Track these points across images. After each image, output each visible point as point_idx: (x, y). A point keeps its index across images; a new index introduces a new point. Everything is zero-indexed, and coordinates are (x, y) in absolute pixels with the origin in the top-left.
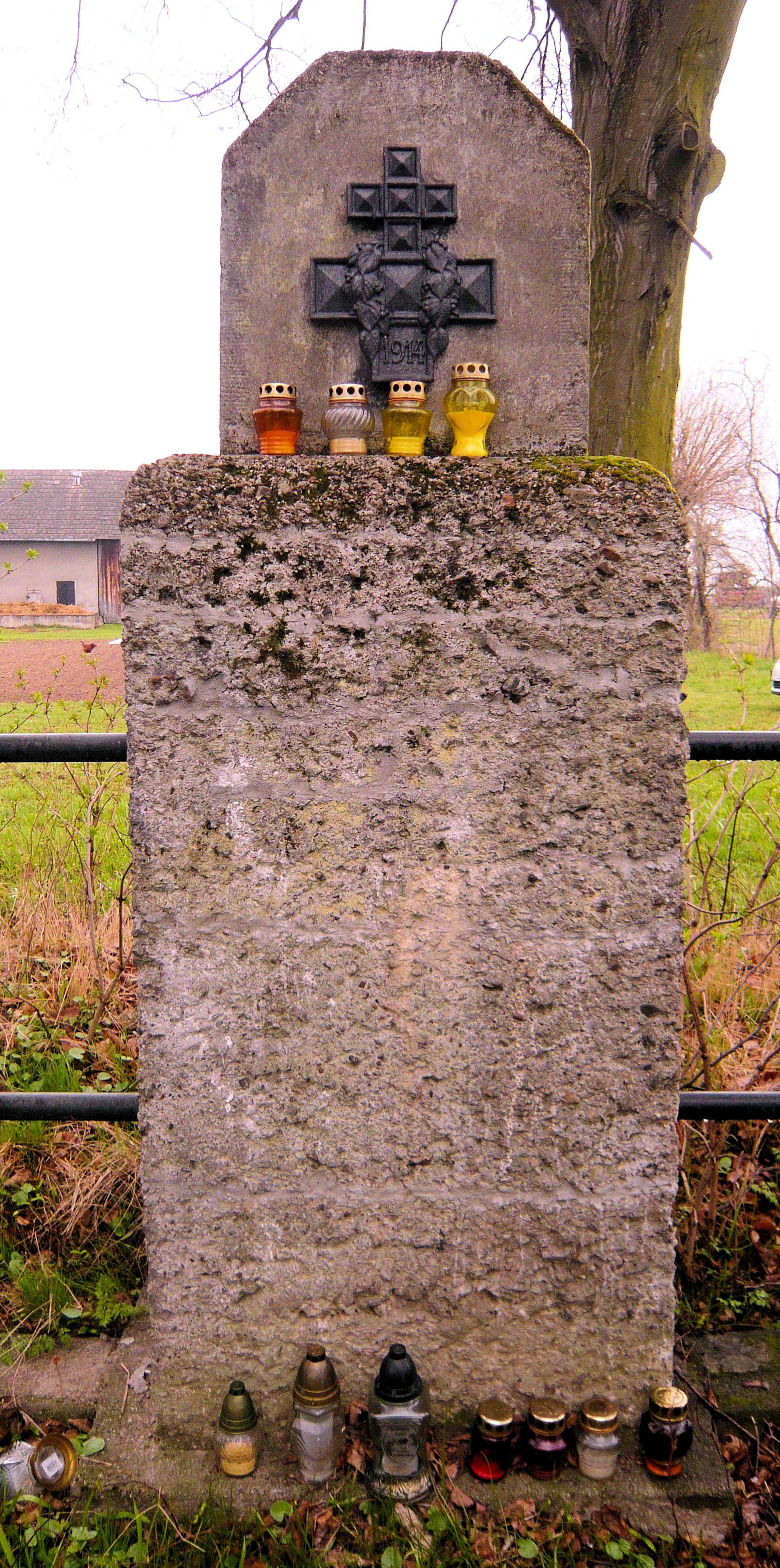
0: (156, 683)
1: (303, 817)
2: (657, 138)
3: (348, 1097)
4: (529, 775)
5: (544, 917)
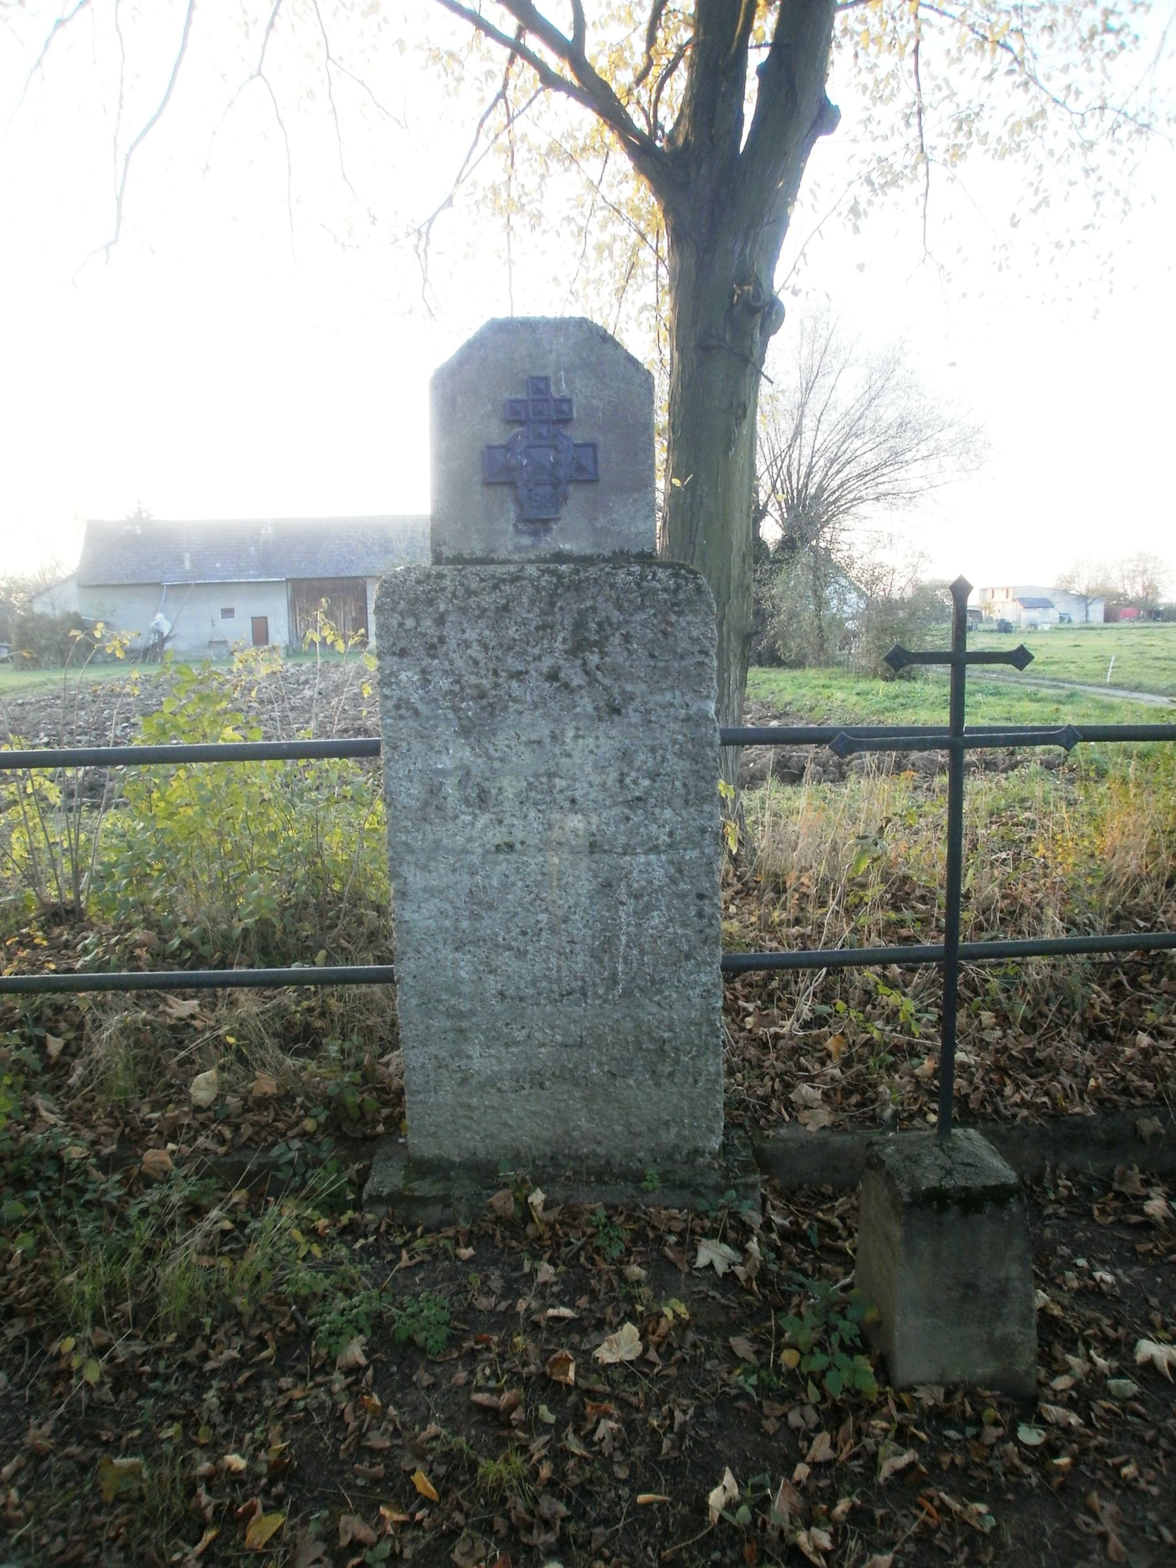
1: (487, 785)
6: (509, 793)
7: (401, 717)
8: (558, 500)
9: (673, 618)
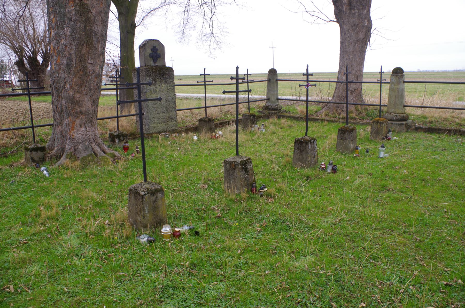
4: (167, 87)
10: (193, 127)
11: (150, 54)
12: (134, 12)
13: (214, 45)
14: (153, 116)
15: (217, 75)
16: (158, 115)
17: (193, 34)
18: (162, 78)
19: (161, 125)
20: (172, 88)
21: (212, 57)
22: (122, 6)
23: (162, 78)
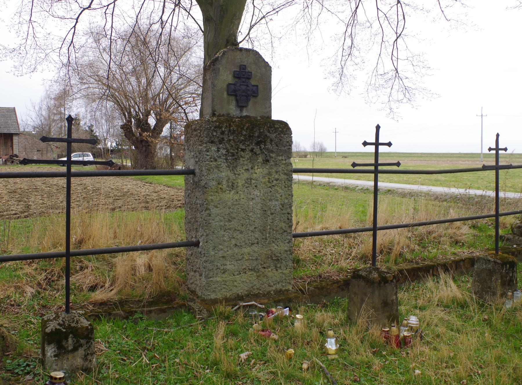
0: (211, 158)
1: (234, 182)
2: (227, 40)
3: (241, 232)
4: (270, 174)
5: (272, 198)
6: (240, 184)
7: (212, 161)
8: (248, 101)
9: (283, 135)
10: (338, 282)
11: (229, 85)
12: (235, 15)
13: (397, 95)
14: (221, 254)
15: (396, 153)
16: (236, 250)
17: (360, 76)
18: (257, 150)
19: (245, 277)
20: (283, 177)
21: (393, 118)
22: (211, 4)
23: (257, 150)
